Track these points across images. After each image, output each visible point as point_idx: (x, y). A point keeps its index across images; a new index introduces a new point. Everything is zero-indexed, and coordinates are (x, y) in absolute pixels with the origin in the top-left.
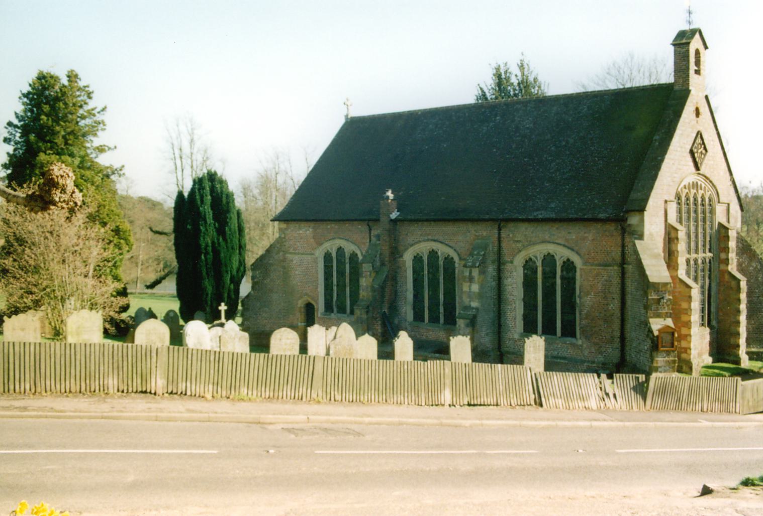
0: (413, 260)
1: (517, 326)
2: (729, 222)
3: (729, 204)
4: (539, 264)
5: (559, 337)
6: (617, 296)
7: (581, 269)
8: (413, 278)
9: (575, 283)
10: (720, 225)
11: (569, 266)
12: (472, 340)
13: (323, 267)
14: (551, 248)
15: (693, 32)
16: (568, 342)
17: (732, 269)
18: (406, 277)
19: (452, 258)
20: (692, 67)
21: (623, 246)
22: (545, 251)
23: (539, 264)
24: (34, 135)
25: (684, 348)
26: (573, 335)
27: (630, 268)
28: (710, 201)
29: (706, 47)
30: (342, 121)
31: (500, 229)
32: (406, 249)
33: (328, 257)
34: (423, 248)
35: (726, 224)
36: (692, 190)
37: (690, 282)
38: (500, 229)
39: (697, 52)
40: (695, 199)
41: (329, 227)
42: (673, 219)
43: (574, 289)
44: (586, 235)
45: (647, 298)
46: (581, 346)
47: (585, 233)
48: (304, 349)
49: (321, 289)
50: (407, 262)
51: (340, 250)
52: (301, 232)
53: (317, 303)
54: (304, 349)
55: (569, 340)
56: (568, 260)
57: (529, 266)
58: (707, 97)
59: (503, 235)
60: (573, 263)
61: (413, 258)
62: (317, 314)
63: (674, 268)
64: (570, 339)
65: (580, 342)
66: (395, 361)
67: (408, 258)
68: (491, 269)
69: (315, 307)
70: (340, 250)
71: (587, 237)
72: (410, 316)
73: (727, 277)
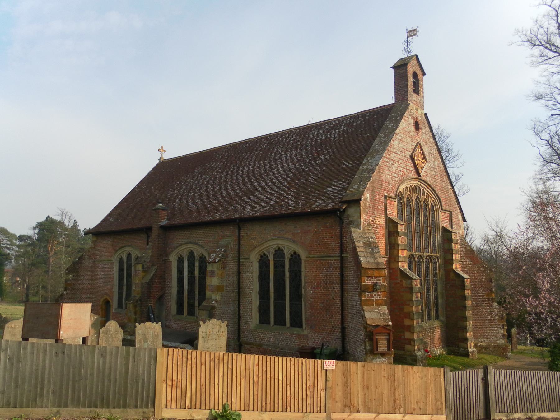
0: (178, 261)
1: (253, 317)
2: (452, 228)
3: (451, 212)
4: (271, 258)
5: (288, 328)
6: (337, 286)
7: (305, 261)
8: (178, 276)
9: (301, 275)
10: (444, 229)
11: (295, 259)
12: (407, 344)
13: (118, 270)
14: (280, 243)
15: (411, 58)
16: (295, 332)
17: (456, 268)
18: (171, 275)
19: (205, 257)
20: (410, 88)
21: (342, 237)
22: (276, 246)
23: (271, 258)
24: (550, 359)
25: (408, 339)
26: (301, 326)
27: (348, 255)
28: (433, 207)
29: (424, 74)
30: (157, 162)
31: (240, 229)
32: (172, 251)
33: (121, 262)
34: (184, 250)
35: (450, 229)
36: (414, 194)
37: (411, 274)
38: (240, 229)
39: (415, 75)
40: (418, 203)
41: (122, 237)
42: (393, 213)
43: (300, 280)
44: (309, 228)
45: (361, 285)
46: (307, 336)
47: (309, 226)
48: (129, 342)
49: (116, 289)
50: (172, 262)
51: (279, 253)
52: (105, 242)
53: (112, 300)
54: (129, 342)
55: (296, 330)
56: (295, 253)
57: (263, 262)
58: (426, 115)
59: (242, 234)
60: (299, 255)
61: (177, 258)
62: (112, 311)
63: (395, 261)
64: (297, 329)
65: (305, 332)
66: (199, 352)
67: (173, 259)
68: (232, 266)
69: (111, 304)
70: (279, 253)
71: (309, 230)
72: (173, 306)
73: (452, 274)
